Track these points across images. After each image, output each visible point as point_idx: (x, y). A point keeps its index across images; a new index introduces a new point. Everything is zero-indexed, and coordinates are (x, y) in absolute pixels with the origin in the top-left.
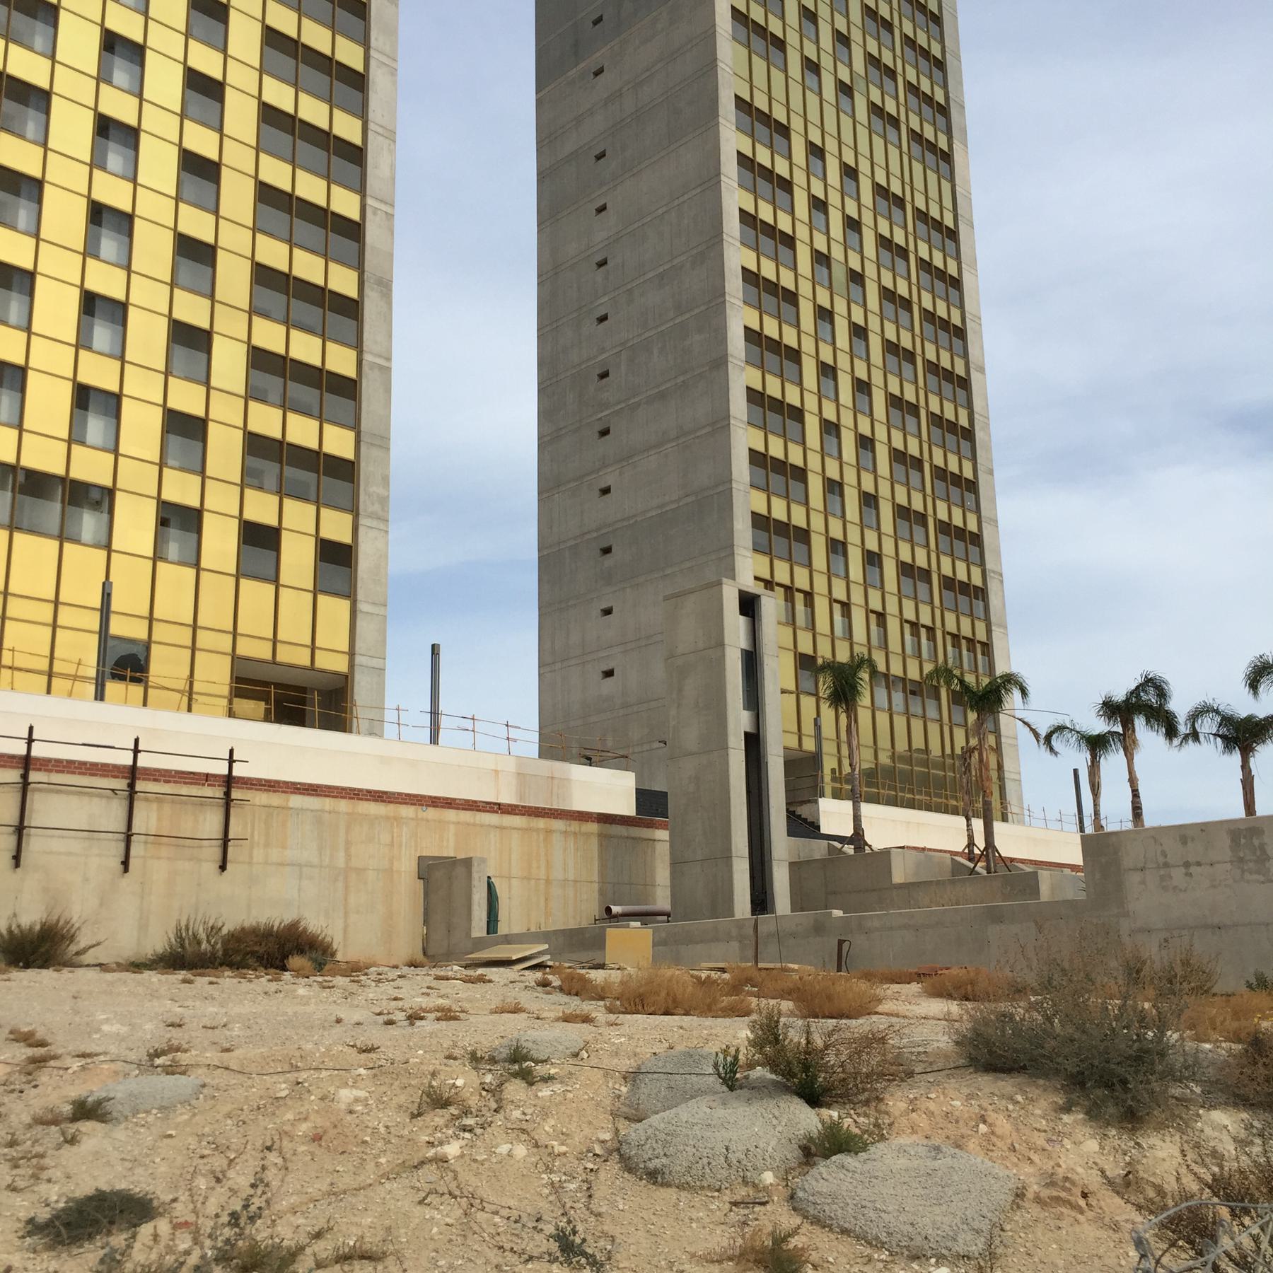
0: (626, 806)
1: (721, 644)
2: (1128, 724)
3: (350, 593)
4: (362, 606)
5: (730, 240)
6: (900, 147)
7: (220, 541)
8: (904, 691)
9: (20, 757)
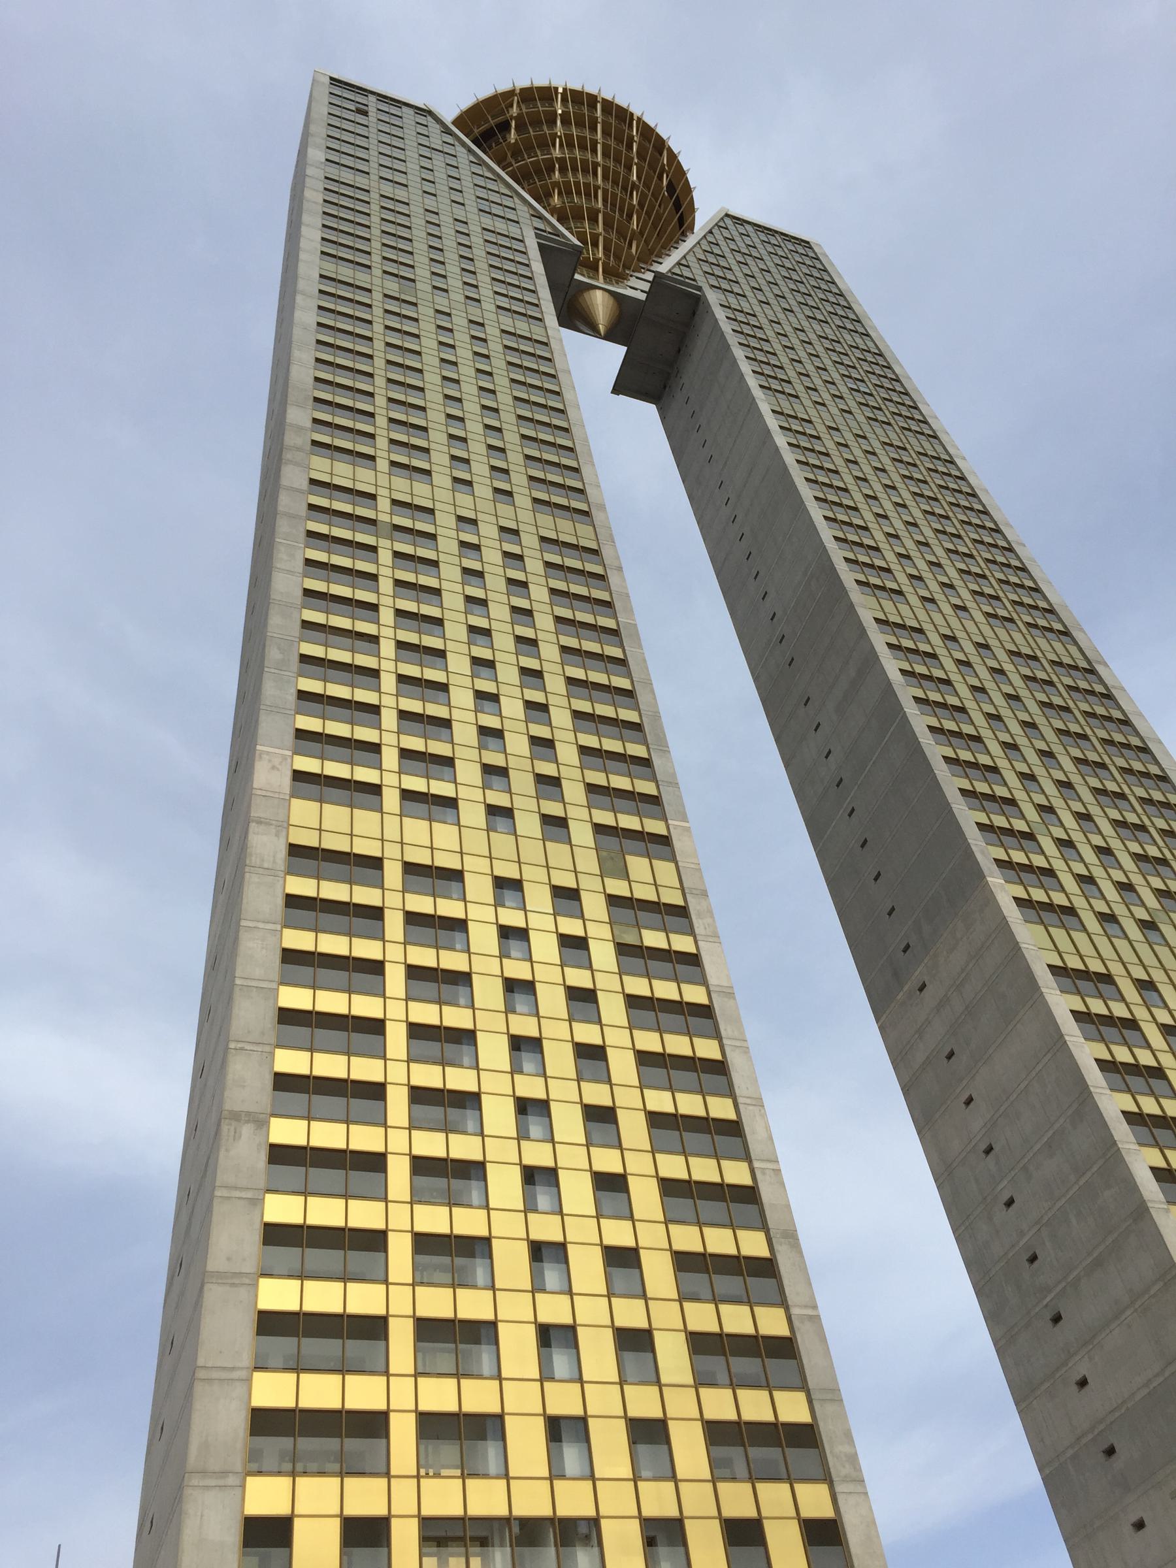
5: (1098, 1090)
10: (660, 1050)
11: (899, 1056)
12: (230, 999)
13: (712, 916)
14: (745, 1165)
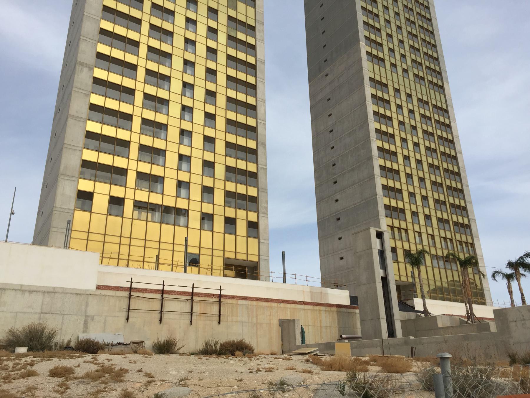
0: (347, 302)
1: (371, 248)
2: (516, 270)
3: (257, 237)
4: (261, 241)
6: (425, 86)
7: (219, 224)
8: (443, 261)
9: (128, 288)
10: (235, 76)
11: (312, 96)
12: (82, 20)
13: (263, 33)
14: (255, 165)
